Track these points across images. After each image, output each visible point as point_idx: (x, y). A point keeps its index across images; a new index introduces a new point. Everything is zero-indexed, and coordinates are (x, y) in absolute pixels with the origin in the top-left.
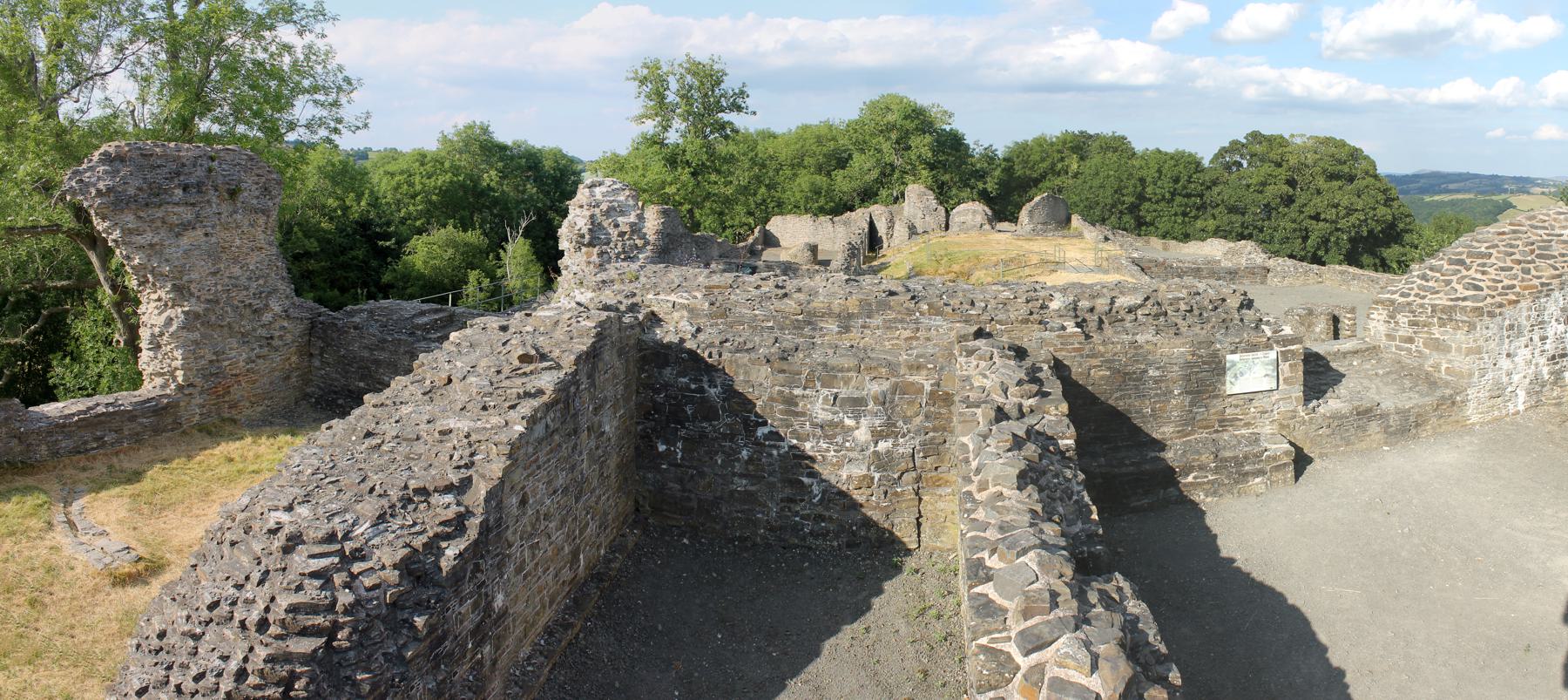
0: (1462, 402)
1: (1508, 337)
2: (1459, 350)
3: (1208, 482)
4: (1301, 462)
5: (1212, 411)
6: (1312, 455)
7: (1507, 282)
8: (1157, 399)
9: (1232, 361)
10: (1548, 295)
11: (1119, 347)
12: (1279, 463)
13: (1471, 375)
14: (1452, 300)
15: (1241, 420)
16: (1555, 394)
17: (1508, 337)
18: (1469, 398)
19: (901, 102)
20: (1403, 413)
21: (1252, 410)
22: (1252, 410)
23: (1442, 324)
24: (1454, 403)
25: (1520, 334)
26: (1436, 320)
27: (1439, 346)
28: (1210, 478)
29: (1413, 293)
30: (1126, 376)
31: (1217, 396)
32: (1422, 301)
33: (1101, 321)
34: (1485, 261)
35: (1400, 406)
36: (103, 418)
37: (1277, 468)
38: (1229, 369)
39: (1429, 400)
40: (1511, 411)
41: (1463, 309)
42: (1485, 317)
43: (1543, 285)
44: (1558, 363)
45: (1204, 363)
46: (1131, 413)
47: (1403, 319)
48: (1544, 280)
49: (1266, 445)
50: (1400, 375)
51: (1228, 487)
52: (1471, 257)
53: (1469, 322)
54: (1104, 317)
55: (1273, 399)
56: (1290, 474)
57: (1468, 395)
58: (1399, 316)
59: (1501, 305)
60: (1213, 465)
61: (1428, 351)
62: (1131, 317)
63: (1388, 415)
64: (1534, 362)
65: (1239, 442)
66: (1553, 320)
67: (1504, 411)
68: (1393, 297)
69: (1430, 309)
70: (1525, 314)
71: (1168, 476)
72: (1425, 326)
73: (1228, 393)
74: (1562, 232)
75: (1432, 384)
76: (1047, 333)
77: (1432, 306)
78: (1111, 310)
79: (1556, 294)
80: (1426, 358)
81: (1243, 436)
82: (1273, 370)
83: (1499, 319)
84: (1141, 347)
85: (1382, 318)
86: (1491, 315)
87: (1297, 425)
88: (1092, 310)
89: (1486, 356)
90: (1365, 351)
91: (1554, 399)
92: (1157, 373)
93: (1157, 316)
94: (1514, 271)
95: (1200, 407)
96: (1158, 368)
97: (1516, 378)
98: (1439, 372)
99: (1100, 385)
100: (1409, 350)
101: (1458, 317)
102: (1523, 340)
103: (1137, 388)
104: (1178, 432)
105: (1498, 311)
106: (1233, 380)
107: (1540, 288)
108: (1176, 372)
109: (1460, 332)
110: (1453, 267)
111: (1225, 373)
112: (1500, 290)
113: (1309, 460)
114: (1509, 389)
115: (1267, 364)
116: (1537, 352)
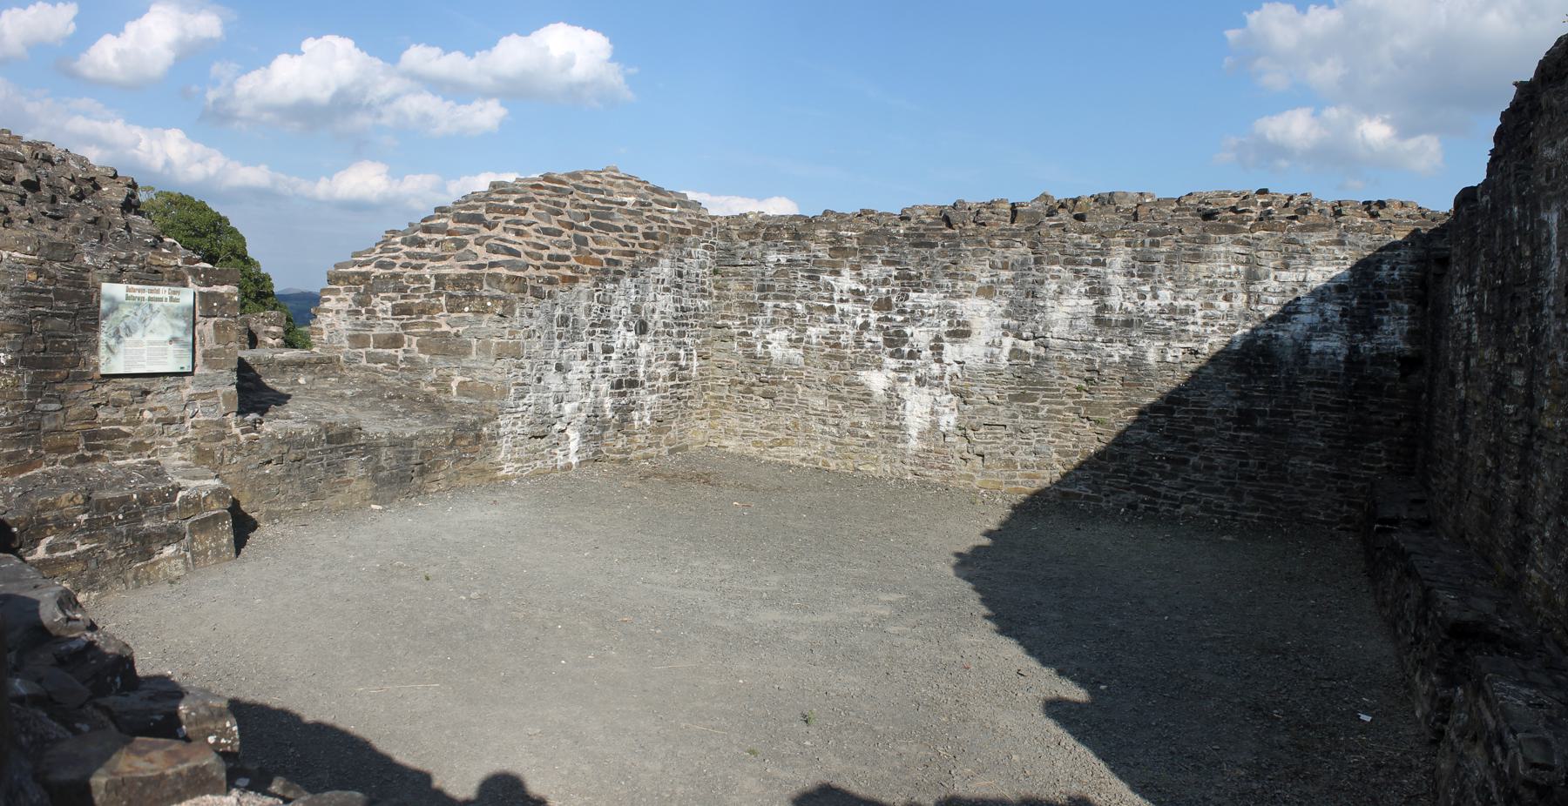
0: (491, 437)
1: (560, 337)
2: (485, 349)
4: (243, 527)
5: (73, 412)
6: (254, 515)
7: (554, 250)
9: (112, 299)
10: (615, 281)
12: (205, 515)
13: (504, 393)
14: (470, 267)
15: (127, 435)
16: (619, 445)
17: (560, 337)
18: (502, 430)
20: (401, 445)
21: (147, 415)
22: (147, 415)
23: (455, 306)
24: (478, 437)
25: (575, 336)
26: (443, 300)
27: (448, 347)
28: (81, 548)
29: (399, 262)
31: (81, 378)
32: (417, 272)
34: (517, 217)
35: (396, 432)
37: (204, 525)
38: (105, 316)
39: (439, 429)
40: (560, 464)
41: (495, 278)
42: (528, 297)
43: (609, 261)
44: (624, 394)
45: (60, 296)
47: (382, 305)
48: (609, 256)
49: (177, 480)
50: (381, 397)
51: (115, 565)
52: (494, 211)
53: (504, 299)
55: (185, 393)
56: (227, 539)
57: (499, 426)
58: (375, 300)
59: (551, 281)
60: (83, 517)
61: (426, 357)
63: (378, 447)
64: (593, 386)
65: (130, 477)
66: (621, 323)
67: (549, 463)
68: (364, 269)
69: (433, 282)
70: (584, 303)
72: (423, 312)
73: (103, 371)
74: (625, 199)
75: (436, 408)
77: (437, 277)
79: (627, 281)
80: (424, 370)
81: (134, 467)
82: (186, 333)
83: (548, 302)
85: (344, 306)
86: (538, 295)
87: (228, 454)
89: (527, 363)
90: (317, 364)
91: (619, 452)
94: (564, 238)
97: (568, 408)
98: (447, 391)
100: (392, 361)
101: (486, 290)
102: (581, 346)
105: (546, 288)
106: (112, 342)
107: (605, 266)
109: (486, 317)
110: (464, 225)
111: (97, 324)
112: (546, 260)
113: (253, 525)
114: (558, 426)
115: (176, 316)
116: (598, 369)
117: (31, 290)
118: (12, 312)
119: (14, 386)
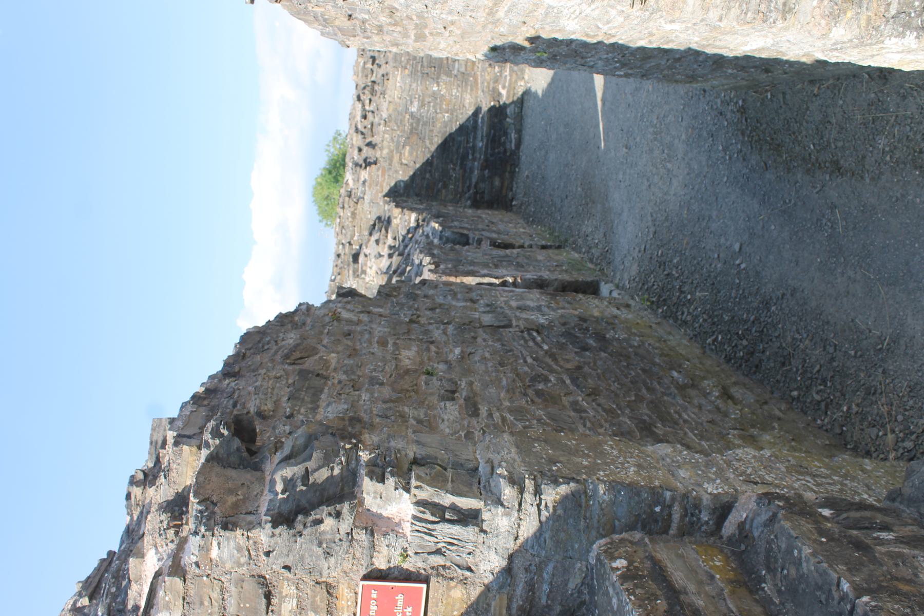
3: (511, 75)
8: (438, 107)
11: (386, 136)
19: (321, 184)
30: (413, 131)
33: (369, 144)
36: (89, 581)
46: (446, 132)
54: (367, 141)
62: (370, 115)
71: (498, 112)
76: (366, 197)
78: (362, 133)
84: (390, 116)
88: (360, 150)
92: (416, 104)
93: (373, 92)
95: (454, 67)
96: (412, 103)
99: (417, 157)
103: (425, 124)
104: (472, 90)
108: (417, 87)
117: (412, 72)
118: (419, 82)
119: (446, 84)
